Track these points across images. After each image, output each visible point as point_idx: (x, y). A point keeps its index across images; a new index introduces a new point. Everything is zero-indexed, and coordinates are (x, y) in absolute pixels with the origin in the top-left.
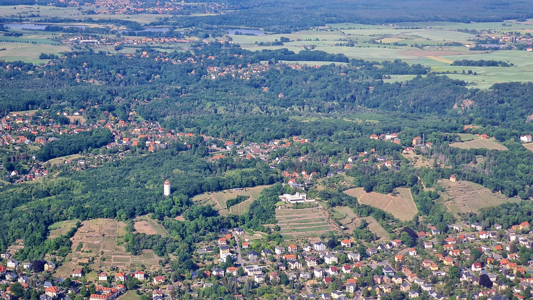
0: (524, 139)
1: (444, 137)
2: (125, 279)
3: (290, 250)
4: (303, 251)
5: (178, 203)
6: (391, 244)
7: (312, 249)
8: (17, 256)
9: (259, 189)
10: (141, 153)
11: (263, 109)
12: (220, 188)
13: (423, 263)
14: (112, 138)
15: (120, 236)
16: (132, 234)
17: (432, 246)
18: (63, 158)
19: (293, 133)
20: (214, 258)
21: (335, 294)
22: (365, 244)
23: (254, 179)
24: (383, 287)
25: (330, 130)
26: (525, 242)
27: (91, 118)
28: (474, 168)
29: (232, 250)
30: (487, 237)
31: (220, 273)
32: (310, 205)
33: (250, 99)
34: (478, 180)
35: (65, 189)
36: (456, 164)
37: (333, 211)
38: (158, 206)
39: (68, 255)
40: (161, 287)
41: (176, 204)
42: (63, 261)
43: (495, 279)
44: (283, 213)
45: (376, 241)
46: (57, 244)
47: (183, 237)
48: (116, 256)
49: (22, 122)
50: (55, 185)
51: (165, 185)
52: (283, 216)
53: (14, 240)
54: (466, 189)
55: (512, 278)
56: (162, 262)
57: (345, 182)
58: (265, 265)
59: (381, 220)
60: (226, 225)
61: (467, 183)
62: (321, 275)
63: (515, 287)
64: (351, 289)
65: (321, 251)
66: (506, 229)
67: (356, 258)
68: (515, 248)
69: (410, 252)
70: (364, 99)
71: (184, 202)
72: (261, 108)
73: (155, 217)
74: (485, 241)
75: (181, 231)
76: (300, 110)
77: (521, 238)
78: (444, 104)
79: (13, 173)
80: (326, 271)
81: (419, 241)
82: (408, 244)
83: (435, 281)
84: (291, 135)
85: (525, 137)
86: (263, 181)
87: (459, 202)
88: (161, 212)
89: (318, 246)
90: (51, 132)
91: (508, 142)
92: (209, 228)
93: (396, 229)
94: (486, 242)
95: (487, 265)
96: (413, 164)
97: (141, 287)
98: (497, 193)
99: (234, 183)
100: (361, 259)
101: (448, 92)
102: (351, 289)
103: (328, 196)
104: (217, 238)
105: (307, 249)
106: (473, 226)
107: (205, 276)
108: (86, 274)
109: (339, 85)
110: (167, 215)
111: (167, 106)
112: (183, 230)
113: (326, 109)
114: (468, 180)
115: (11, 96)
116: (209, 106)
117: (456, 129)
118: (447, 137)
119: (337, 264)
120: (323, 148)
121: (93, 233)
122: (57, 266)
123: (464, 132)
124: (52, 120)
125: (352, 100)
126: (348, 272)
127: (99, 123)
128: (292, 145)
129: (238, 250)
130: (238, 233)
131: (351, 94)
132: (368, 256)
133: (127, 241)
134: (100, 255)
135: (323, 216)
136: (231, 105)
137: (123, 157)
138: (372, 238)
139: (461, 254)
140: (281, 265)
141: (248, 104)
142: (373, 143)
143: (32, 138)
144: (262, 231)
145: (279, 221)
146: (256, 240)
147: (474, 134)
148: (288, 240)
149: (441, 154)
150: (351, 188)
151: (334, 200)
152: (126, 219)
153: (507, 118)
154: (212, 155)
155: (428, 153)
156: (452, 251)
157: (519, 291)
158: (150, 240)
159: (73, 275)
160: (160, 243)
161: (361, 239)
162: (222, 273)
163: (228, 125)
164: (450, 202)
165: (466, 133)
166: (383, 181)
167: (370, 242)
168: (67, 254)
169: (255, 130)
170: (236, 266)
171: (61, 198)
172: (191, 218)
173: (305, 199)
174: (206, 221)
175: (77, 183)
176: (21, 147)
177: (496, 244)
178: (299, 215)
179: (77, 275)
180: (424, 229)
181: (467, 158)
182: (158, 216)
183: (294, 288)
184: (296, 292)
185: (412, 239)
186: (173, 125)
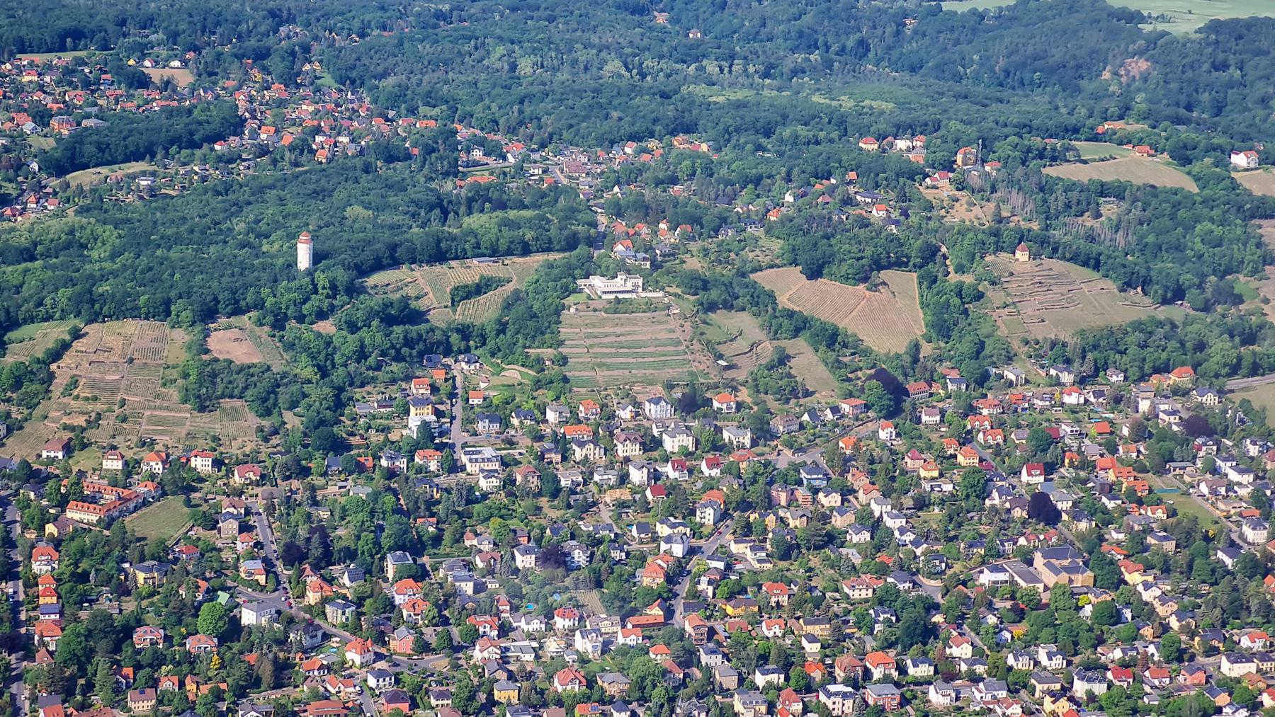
0: (1239, 160)
1: (1037, 150)
2: (164, 468)
3: (583, 414)
4: (614, 416)
5: (324, 288)
6: (835, 410)
7: (637, 414)
9: (537, 259)
10: (296, 164)
11: (631, 67)
12: (439, 255)
13: (907, 459)
14: (237, 126)
15: (170, 363)
16: (200, 360)
17: (938, 418)
18: (104, 170)
19: (679, 128)
20: (393, 427)
21: (665, 526)
22: (773, 405)
23: (529, 235)
24: (788, 515)
25: (769, 123)
26: (1172, 417)
27: (205, 75)
28: (1092, 228)
29: (441, 407)
30: (1082, 401)
31: (397, 463)
32: (650, 306)
33: (604, 40)
35: (74, 244)
36: (1048, 217)
37: (705, 322)
38: (275, 296)
39: (41, 406)
40: (251, 490)
41: (320, 291)
43: (1070, 503)
45: (802, 401)
46: (16, 377)
47: (324, 372)
49: (35, 78)
50: (51, 236)
52: (578, 330)
54: (1052, 281)
55: (1110, 505)
56: (262, 431)
57: (758, 252)
58: (515, 449)
59: (822, 348)
60: (438, 347)
61: (1057, 265)
63: (1113, 526)
64: (708, 516)
65: (657, 421)
66: (1134, 382)
67: (741, 439)
68: (1141, 432)
69: (880, 431)
70: (890, 48)
71: (340, 288)
72: (626, 66)
73: (264, 322)
74: (1073, 410)
75: (322, 357)
76: (722, 70)
77: (1163, 407)
78: (1079, 67)
80: (659, 469)
81: (907, 405)
82: (881, 411)
83: (922, 504)
84: (673, 133)
85: (1242, 155)
86: (550, 240)
88: (280, 308)
90: (96, 105)
91: (1196, 167)
92: (393, 352)
93: (859, 374)
94: (1077, 412)
95: (1062, 470)
96: (942, 212)
97: (201, 488)
98: (1132, 292)
99: (477, 246)
100: (754, 443)
101: (1093, 38)
102: (706, 515)
103: (699, 284)
104: (408, 378)
105: (626, 414)
106: (1053, 372)
107: (361, 468)
108: (76, 453)
109: (832, 14)
110: (294, 318)
111: (396, 51)
113: (786, 70)
114: (1063, 258)
115: (29, 15)
116: (498, 55)
117: (1076, 130)
118: (1045, 149)
119: (691, 454)
120: (733, 167)
121: (106, 354)
123: (1095, 138)
124: (109, 76)
125: (861, 50)
126: (713, 475)
127: (223, 89)
128: (665, 158)
129: (458, 410)
130: (466, 367)
131: (858, 35)
132: (774, 436)
133: (186, 376)
134: (116, 408)
135: (677, 335)
136: (553, 55)
137: (251, 172)
138: (795, 392)
139: (1005, 441)
140: (550, 451)
141: (594, 51)
142: (855, 159)
143: (42, 117)
144: (523, 366)
145: (567, 343)
146: (504, 386)
147: (1120, 143)
148: (583, 390)
149: (1015, 192)
150: (771, 267)
151: (714, 294)
152: (193, 324)
153: (1229, 108)
154: (465, 175)
155: (984, 187)
156: (984, 433)
157: (1121, 536)
158: (241, 376)
159: (44, 454)
160: (265, 384)
161: (766, 393)
162: (402, 463)
163: (527, 101)
165: (1101, 141)
166: (850, 252)
167: (787, 401)
168: (39, 403)
169: (585, 119)
170: (440, 447)
171: (54, 268)
172: (353, 327)
173: (640, 290)
174: (387, 335)
175: (109, 233)
176: (9, 140)
177: (1101, 417)
178: (618, 330)
179: (52, 454)
180: (927, 375)
181: (1079, 202)
182: (270, 318)
183: (569, 506)
184: (573, 517)
185: (890, 400)
186: (397, 99)
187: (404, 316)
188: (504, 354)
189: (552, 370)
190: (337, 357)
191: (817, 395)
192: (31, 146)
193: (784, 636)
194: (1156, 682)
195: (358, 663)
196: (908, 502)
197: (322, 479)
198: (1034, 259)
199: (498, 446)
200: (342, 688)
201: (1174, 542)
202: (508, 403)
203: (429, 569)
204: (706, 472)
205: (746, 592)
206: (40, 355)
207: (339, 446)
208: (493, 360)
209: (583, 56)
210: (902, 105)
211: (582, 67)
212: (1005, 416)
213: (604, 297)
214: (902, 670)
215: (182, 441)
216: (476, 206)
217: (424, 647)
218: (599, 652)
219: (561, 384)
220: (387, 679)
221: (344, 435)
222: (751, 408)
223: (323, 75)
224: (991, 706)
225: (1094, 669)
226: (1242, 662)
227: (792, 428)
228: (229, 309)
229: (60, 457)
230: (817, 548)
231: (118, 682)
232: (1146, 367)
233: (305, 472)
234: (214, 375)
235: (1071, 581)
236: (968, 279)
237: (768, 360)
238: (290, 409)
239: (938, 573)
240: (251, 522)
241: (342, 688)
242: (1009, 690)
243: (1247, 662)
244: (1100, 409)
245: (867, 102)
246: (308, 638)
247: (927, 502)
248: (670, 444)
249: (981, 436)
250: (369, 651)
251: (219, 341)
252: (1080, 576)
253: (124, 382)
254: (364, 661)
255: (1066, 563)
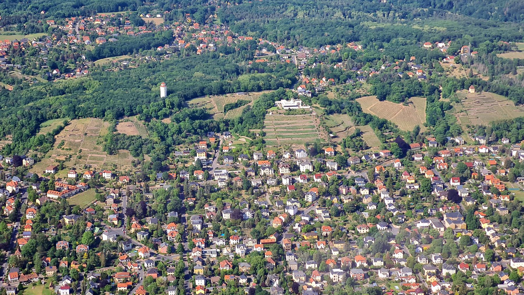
4: (281, 157)
5: (168, 105)
6: (377, 155)
7: (292, 156)
8: (4, 150)
13: (403, 175)
17: (421, 158)
18: (111, 59)
28: (512, 79)
30: (487, 151)
31: (185, 176)
32: (304, 112)
34: (504, 92)
37: (326, 118)
39: (49, 152)
41: (167, 106)
42: (43, 158)
43: (468, 194)
44: (273, 118)
45: (365, 151)
47: (163, 139)
48: (93, 155)
50: (73, 85)
51: (161, 88)
53: (5, 135)
56: (134, 162)
57: (361, 90)
61: (488, 94)
62: (288, 182)
64: (309, 198)
66: (513, 143)
67: (333, 167)
72: (344, 14)
74: (483, 155)
75: (162, 133)
79: (55, 72)
82: (397, 155)
83: (404, 194)
86: (270, 85)
87: (472, 114)
88: (149, 113)
89: (298, 153)
92: (193, 131)
94: (484, 156)
97: (105, 185)
99: (239, 88)
100: (339, 168)
102: (309, 198)
103: (327, 103)
104: (198, 141)
105: (287, 156)
108: (60, 171)
112: (165, 132)
114: (492, 92)
121: (77, 131)
122: (35, 162)
126: (318, 181)
130: (225, 137)
133: (106, 140)
136: (314, 10)
137: (169, 59)
140: (250, 171)
143: (93, 38)
144: (247, 136)
145: (266, 127)
146: (238, 144)
148: (271, 146)
150: (365, 96)
151: (333, 107)
159: (47, 171)
160: (138, 143)
162: (187, 176)
164: (462, 113)
168: (49, 151)
172: (178, 121)
178: (289, 122)
179: (49, 171)
180: (421, 140)
181: (507, 68)
182: (144, 117)
183: (253, 194)
185: (401, 150)
187: (202, 116)
188: (240, 132)
189: (259, 138)
190: (169, 133)
191: (372, 148)
192: (85, 49)
193: (325, 248)
194: (479, 270)
195: (143, 257)
196: (398, 193)
197: (154, 182)
198: (477, 92)
199: (231, 169)
200: (133, 267)
201: (508, 211)
202: (238, 152)
203: (186, 219)
204: (316, 180)
205: (316, 230)
206: (51, 132)
207: (165, 169)
208: (236, 134)
209: (326, 10)
210: (449, 29)
211: (325, 15)
212: (451, 158)
213: (285, 108)
214: (370, 263)
215: (102, 166)
216: (252, 71)
217: (172, 250)
218: (244, 254)
219: (262, 144)
220: (152, 264)
221: (168, 164)
222: (342, 154)
223: (217, 19)
224: (403, 279)
225: (454, 264)
226: (518, 262)
227: (357, 162)
228: (128, 114)
229: (53, 172)
230: (352, 212)
231: (43, 263)
232: (519, 137)
233: (147, 179)
234: (117, 140)
235: (456, 227)
236: (447, 100)
237: (352, 134)
238: (147, 154)
239: (401, 223)
240: (121, 199)
241: (133, 267)
242: (413, 272)
243: (520, 262)
244: (495, 155)
245: (435, 28)
246: (126, 246)
247: (406, 193)
248: (303, 169)
249: (438, 165)
250: (147, 252)
251: (122, 126)
252: (460, 225)
253: (82, 142)
254: (145, 256)
255: (456, 219)
